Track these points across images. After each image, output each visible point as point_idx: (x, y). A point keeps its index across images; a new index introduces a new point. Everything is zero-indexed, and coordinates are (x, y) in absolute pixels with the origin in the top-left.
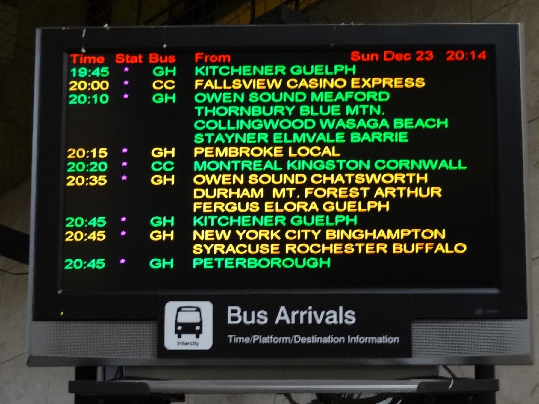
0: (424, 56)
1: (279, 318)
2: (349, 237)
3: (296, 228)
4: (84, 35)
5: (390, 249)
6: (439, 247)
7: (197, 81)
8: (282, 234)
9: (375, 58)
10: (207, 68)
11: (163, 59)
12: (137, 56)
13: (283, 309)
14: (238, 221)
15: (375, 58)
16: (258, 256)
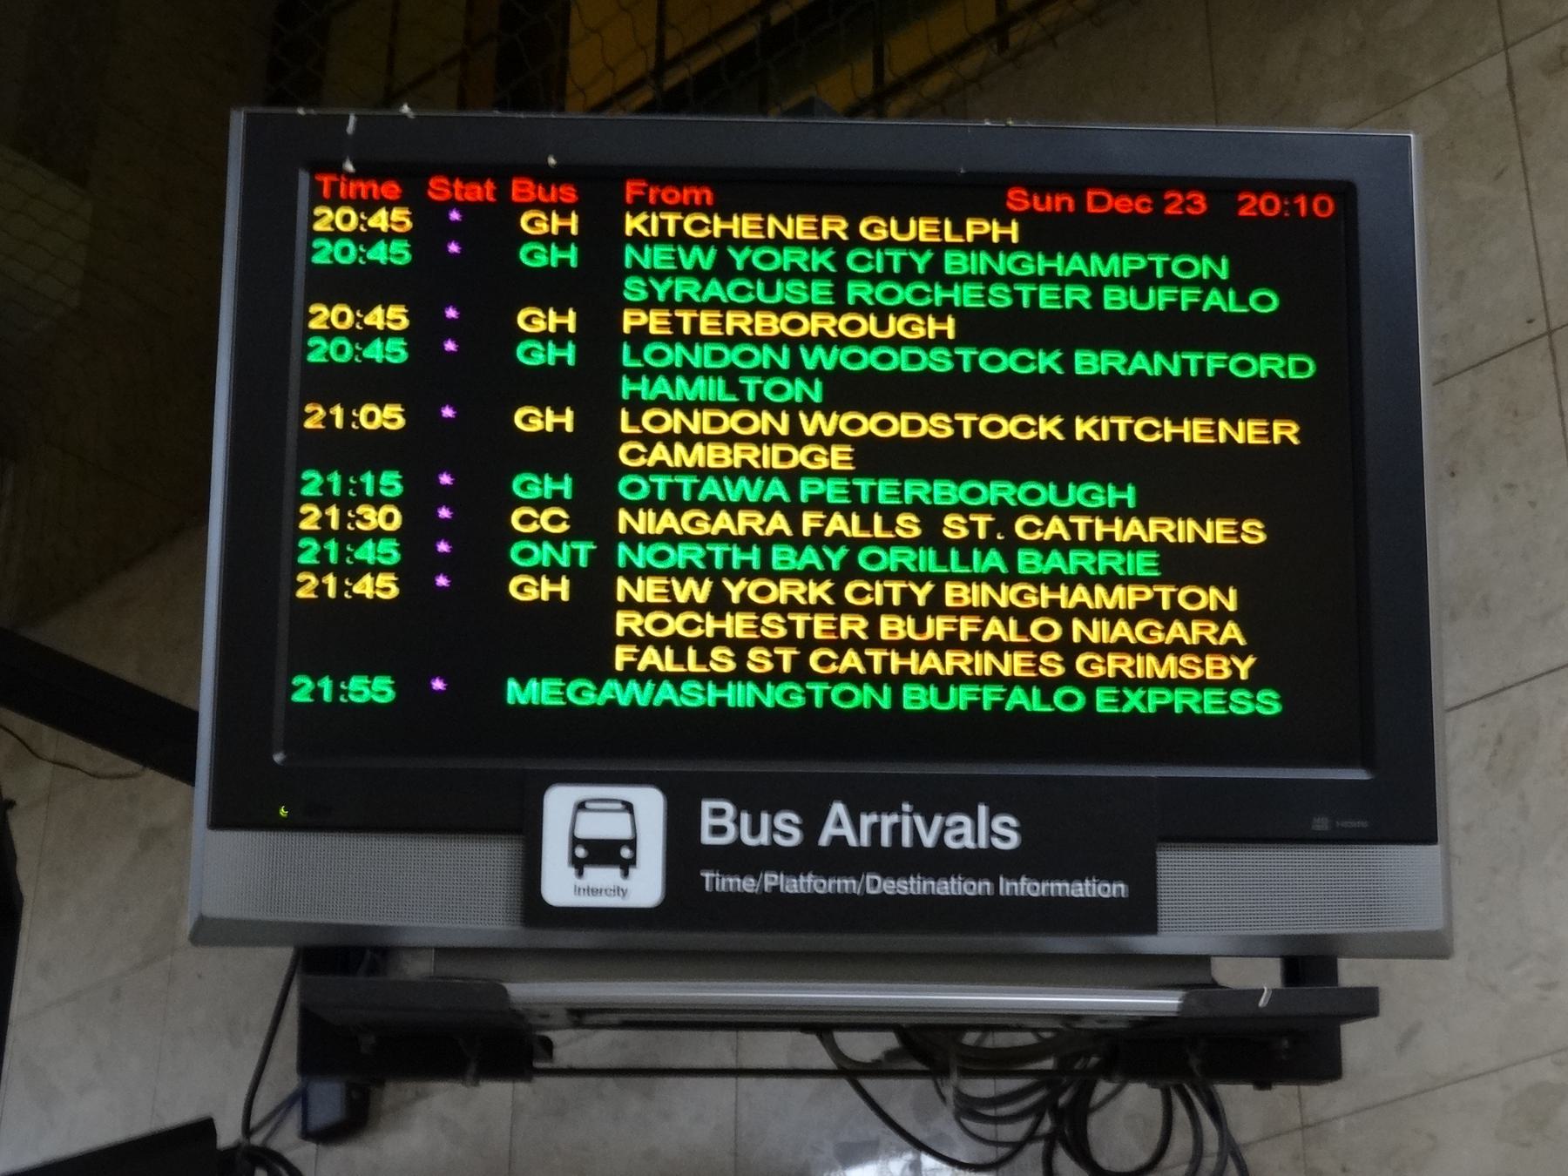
0: (1183, 207)
2: (1000, 271)
3: (873, 246)
5: (1097, 299)
6: (1214, 299)
8: (839, 260)
9: (1064, 204)
10: (654, 219)
11: (548, 192)
12: (482, 183)
13: (838, 809)
15: (1064, 204)
16: (781, 309)
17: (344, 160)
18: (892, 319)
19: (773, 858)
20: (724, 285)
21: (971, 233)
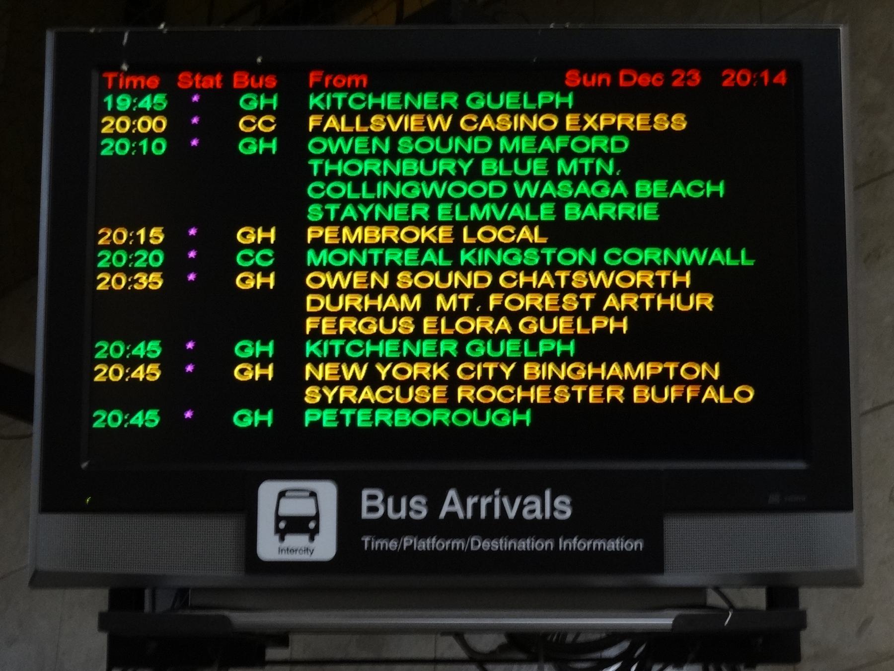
1: (446, 508)
3: (475, 361)
4: (125, 41)
5: (628, 394)
6: (710, 393)
7: (311, 118)
8: (451, 370)
9: (604, 81)
11: (257, 81)
13: (452, 494)
14: (380, 348)
15: (604, 81)
17: (122, 64)
18: (488, 413)
19: (408, 527)
20: (374, 391)
21: (541, 101)
